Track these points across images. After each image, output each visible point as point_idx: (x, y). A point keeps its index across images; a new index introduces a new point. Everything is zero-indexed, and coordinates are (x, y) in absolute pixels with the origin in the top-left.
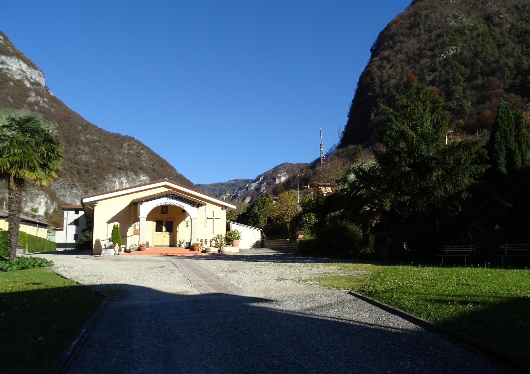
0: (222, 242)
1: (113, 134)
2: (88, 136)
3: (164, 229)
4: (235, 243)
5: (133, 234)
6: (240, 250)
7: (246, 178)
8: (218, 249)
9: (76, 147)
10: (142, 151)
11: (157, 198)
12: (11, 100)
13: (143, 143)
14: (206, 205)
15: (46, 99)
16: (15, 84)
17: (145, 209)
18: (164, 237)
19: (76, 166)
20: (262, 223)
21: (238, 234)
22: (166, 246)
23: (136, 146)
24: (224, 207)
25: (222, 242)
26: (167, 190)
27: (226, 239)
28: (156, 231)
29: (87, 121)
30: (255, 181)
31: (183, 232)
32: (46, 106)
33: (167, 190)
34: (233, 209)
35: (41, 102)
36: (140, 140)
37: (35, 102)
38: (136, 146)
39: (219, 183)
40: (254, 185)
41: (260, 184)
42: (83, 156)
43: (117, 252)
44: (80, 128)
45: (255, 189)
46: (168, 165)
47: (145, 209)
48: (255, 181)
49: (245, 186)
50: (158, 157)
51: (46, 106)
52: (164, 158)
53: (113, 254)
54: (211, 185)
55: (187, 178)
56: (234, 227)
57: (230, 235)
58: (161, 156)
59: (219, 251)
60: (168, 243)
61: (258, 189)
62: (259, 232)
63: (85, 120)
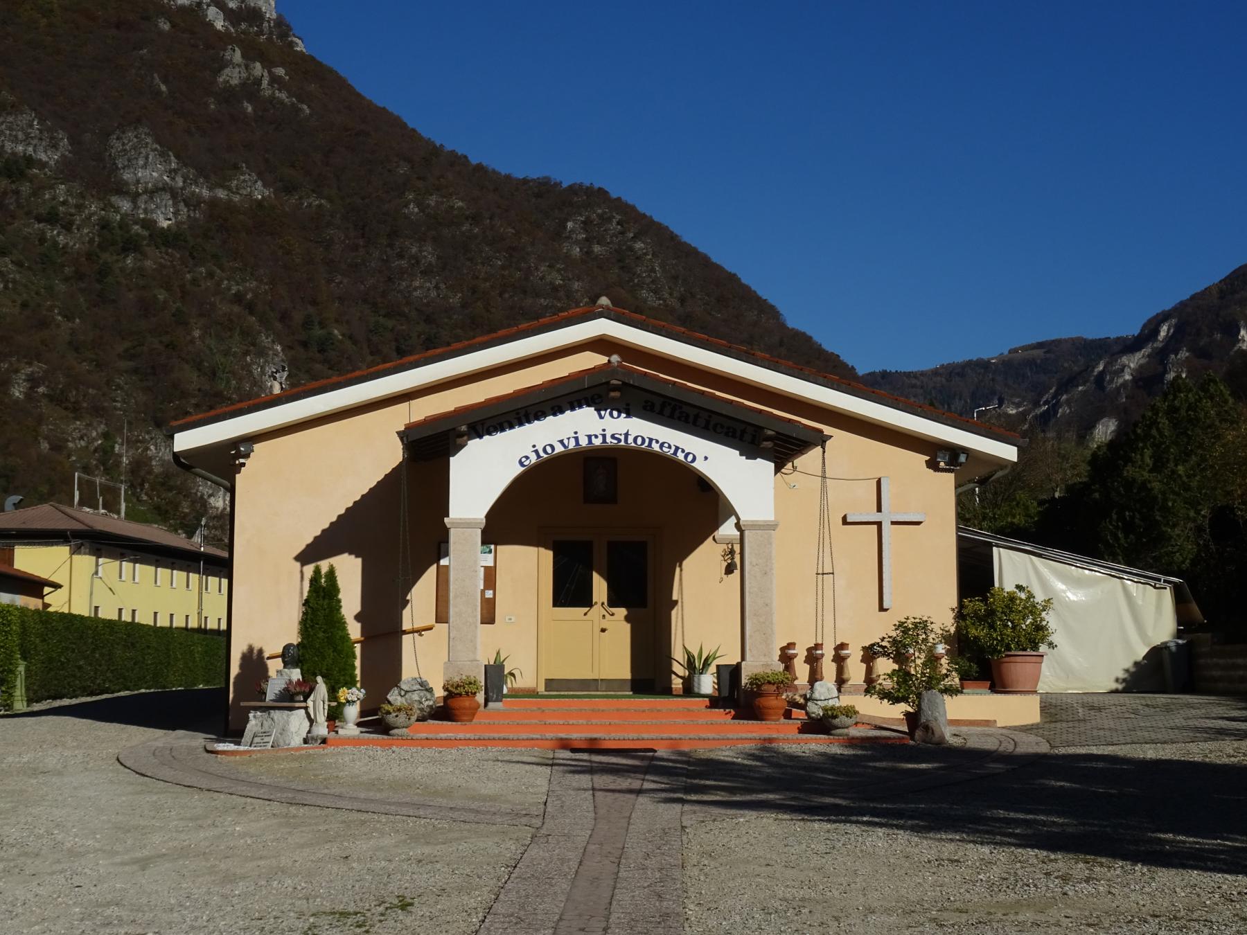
0: (933, 660)
1: (525, 181)
2: (432, 201)
3: (600, 587)
4: (1018, 668)
5: (431, 620)
6: (1053, 709)
7: (1093, 332)
8: (903, 707)
9: (391, 246)
10: (639, 245)
11: (540, 415)
12: (163, 88)
13: (641, 208)
14: (822, 440)
15: (280, 71)
16: (173, 26)
17: (480, 476)
18: (599, 640)
19: (390, 323)
20: (1183, 542)
21: (1032, 609)
22: (611, 684)
23: (614, 226)
24: (940, 455)
25: (933, 660)
26: (601, 360)
27: (960, 643)
28: (558, 602)
29: (428, 142)
30: (1132, 345)
31: (705, 613)
32: (283, 96)
33: (601, 360)
34: (999, 463)
35: (265, 82)
36: (629, 198)
37: (243, 84)
38: (614, 226)
39: (969, 364)
40: (1133, 361)
41: (1161, 356)
42: (417, 284)
43: (322, 729)
44: (403, 169)
45: (1136, 380)
46: (748, 297)
47: (480, 476)
48: (1132, 345)
49: (1089, 367)
50: (705, 261)
51: (283, 96)
52: (730, 266)
53: (297, 741)
54: (935, 372)
55: (828, 346)
56: (1014, 568)
57: (979, 619)
58: (715, 259)
59: (912, 719)
60: (623, 671)
61: (1147, 380)
62: (1167, 596)
63: (420, 138)
